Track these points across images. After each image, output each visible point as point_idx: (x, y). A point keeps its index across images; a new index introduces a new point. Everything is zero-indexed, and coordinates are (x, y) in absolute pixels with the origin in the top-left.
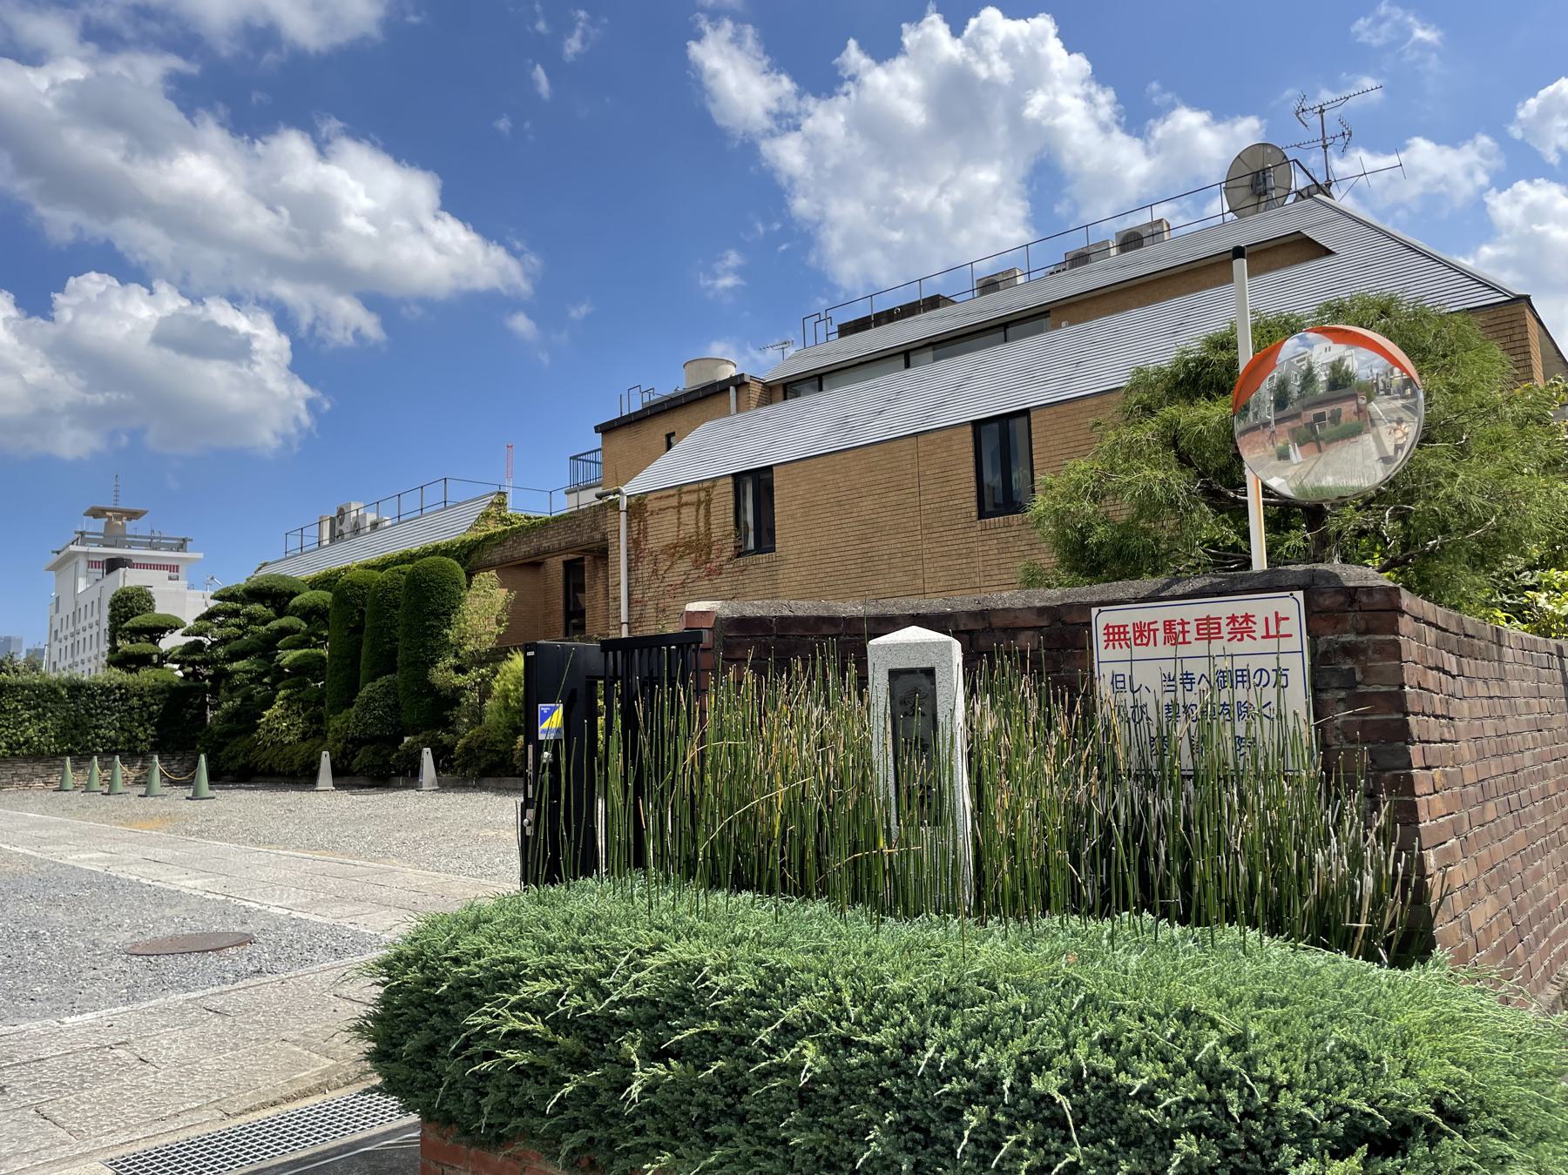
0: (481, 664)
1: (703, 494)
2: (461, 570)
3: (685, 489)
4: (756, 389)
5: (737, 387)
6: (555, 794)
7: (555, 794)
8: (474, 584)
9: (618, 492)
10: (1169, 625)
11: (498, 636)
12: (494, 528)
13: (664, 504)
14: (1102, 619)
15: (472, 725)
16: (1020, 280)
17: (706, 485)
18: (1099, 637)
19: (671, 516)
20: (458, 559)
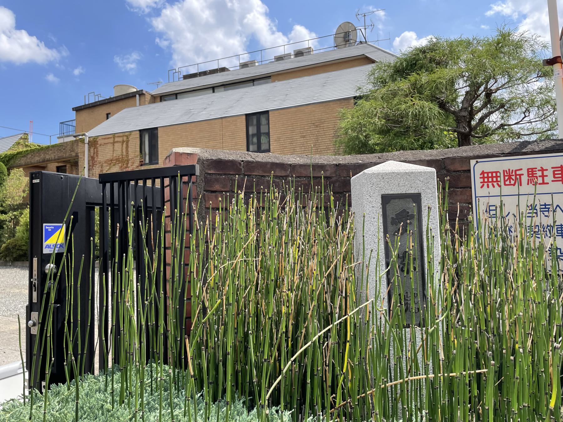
0: (14, 210)
1: (125, 138)
2: (4, 166)
3: (117, 135)
4: (148, 97)
5: (140, 95)
6: (60, 298)
7: (60, 298)
8: (12, 174)
9: (84, 135)
10: (531, 172)
11: (23, 197)
12: (21, 149)
13: (106, 141)
14: (478, 168)
15: (10, 237)
16: (257, 64)
17: (126, 134)
18: (476, 180)
19: (110, 147)
20: (3, 162)
